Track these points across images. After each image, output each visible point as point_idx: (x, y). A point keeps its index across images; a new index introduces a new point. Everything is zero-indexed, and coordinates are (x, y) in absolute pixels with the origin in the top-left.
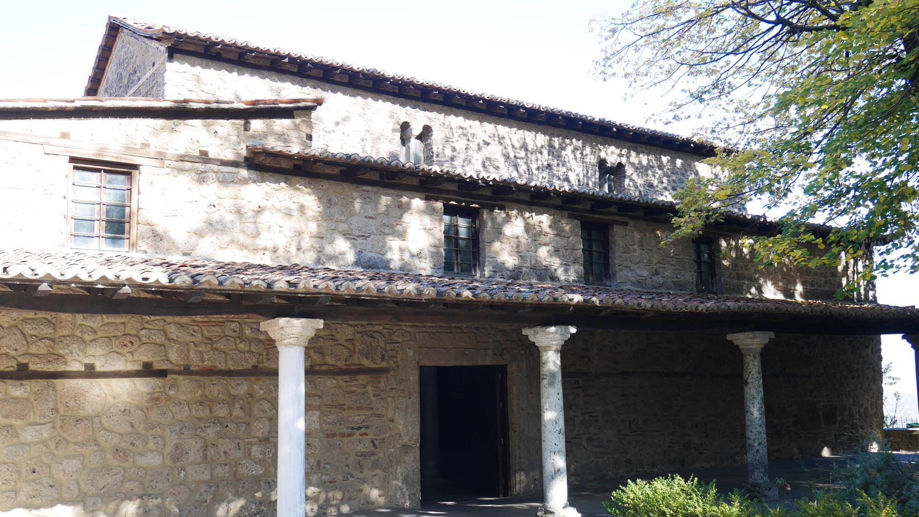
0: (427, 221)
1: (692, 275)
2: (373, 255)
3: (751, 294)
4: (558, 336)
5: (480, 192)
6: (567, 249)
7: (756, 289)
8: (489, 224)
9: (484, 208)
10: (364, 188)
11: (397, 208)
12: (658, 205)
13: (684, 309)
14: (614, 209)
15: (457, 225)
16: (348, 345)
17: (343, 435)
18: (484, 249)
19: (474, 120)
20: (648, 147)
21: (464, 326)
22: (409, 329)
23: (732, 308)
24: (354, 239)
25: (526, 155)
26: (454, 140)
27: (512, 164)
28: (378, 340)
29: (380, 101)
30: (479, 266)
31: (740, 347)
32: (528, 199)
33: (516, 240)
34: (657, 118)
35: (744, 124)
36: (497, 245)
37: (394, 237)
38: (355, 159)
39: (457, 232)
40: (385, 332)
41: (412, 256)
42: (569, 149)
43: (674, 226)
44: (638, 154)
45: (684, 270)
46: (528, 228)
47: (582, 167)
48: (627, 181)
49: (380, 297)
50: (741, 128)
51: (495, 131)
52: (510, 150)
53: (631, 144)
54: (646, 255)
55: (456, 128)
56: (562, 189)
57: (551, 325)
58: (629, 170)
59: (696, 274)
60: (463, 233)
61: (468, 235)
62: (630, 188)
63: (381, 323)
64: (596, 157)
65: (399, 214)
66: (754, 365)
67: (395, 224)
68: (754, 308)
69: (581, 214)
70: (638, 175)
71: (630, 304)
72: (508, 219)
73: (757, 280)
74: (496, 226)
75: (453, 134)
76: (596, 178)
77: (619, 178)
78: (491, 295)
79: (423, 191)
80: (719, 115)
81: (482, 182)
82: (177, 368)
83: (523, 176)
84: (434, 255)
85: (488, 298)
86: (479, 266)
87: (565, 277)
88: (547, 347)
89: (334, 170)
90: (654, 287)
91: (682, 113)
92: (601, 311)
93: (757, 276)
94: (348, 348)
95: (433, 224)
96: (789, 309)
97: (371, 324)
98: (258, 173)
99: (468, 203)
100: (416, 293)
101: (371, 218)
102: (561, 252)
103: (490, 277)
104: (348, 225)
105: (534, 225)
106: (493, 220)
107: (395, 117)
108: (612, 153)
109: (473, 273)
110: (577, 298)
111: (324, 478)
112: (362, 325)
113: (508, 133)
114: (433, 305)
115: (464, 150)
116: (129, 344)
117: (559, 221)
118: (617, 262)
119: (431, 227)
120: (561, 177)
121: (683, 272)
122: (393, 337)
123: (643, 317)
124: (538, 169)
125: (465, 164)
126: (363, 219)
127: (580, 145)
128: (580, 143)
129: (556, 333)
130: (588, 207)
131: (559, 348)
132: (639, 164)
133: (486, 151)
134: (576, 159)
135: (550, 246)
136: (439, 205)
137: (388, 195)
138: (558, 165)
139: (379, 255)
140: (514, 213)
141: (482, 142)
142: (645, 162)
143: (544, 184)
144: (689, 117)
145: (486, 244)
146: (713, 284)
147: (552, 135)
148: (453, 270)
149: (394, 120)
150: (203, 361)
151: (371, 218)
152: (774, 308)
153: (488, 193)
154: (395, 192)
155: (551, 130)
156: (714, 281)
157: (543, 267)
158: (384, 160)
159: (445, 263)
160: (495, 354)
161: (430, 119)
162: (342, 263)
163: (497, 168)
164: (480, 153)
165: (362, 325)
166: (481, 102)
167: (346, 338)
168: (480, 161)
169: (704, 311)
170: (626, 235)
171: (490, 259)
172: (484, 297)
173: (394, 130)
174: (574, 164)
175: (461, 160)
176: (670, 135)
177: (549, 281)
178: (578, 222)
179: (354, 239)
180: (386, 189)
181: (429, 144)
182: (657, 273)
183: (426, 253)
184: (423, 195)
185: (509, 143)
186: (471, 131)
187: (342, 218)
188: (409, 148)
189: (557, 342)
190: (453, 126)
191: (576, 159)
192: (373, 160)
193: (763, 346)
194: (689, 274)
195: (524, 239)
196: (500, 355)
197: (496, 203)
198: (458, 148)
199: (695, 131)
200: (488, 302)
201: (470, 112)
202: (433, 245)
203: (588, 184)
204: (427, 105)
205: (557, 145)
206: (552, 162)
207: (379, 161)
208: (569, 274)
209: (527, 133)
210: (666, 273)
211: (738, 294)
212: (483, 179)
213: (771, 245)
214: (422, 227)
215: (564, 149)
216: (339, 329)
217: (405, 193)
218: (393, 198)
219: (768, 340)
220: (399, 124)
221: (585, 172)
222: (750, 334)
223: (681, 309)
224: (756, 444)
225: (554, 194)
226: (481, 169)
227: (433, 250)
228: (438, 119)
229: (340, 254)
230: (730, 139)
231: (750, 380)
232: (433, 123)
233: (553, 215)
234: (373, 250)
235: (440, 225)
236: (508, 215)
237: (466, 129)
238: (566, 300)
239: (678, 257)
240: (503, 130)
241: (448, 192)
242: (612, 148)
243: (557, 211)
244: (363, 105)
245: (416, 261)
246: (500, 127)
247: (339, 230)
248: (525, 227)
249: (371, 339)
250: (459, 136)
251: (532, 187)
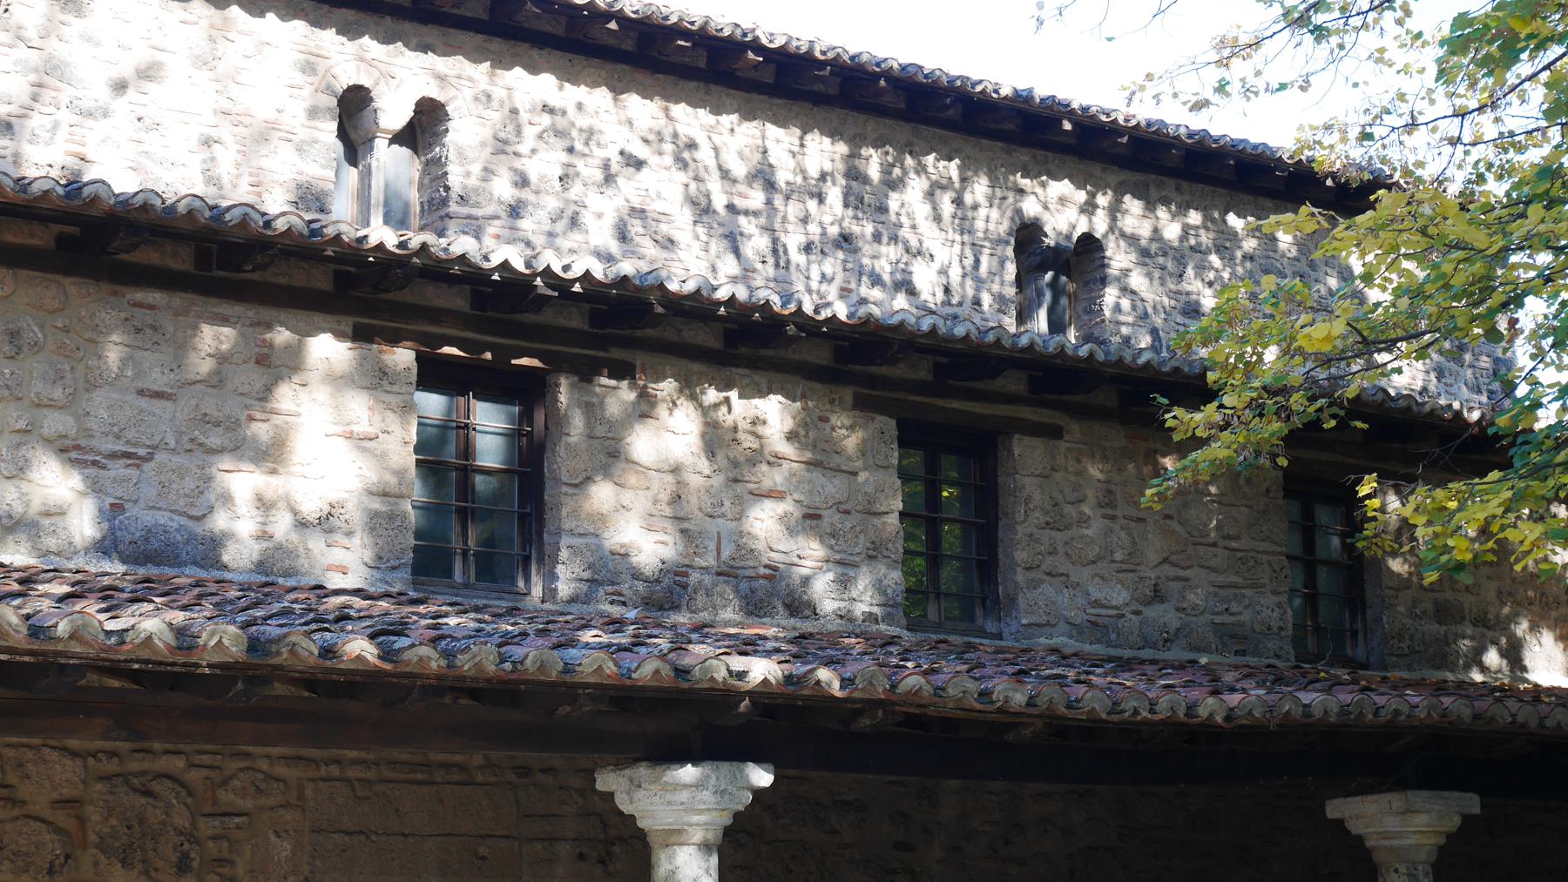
0: (360, 409)
1: (1279, 605)
2: (162, 518)
3: (1484, 669)
4: (706, 796)
5: (547, 317)
6: (847, 512)
7: (1503, 654)
8: (577, 424)
9: (559, 370)
10: (139, 295)
11: (251, 365)
12: (1158, 372)
13: (1145, 714)
14: (1013, 382)
15: (467, 426)
16: (63, 819)
18: (559, 506)
19: (594, 84)
20: (1185, 185)
21: (477, 758)
22: (281, 770)
23: (1317, 713)
24: (95, 463)
25: (769, 202)
26: (524, 148)
27: (721, 231)
28: (169, 805)
29: (271, 16)
30: (541, 561)
31: (1369, 843)
32: (716, 343)
33: (670, 478)
34: (1165, 88)
35: (1461, 114)
36: (602, 494)
37: (241, 459)
38: (95, 199)
39: (467, 450)
40: (194, 776)
41: (302, 524)
42: (916, 186)
43: (1176, 437)
44: (1150, 206)
45: (1252, 586)
46: (715, 439)
47: (957, 247)
48: (1110, 295)
49: (44, 653)
50: (1451, 127)
51: (663, 121)
52: (715, 186)
53: (1125, 175)
54: (1123, 534)
55: (532, 111)
56: (825, 314)
57: (681, 758)
58: (1119, 258)
59: (1297, 602)
60: (490, 450)
61: (509, 459)
62: (1122, 318)
63: (182, 747)
64: (1009, 213)
65: (258, 385)
67: (243, 418)
68: (1397, 712)
69: (900, 395)
70: (1149, 275)
71: (951, 691)
72: (645, 408)
73: (1504, 625)
74: (600, 431)
75: (519, 132)
76: (1002, 283)
77: (1087, 283)
78: (448, 655)
79: (346, 312)
80: (1381, 86)
81: (548, 285)
83: (754, 271)
84: (378, 523)
85: (436, 663)
86: (541, 561)
87: (835, 605)
88: (672, 832)
89: (32, 235)
90: (1148, 643)
91: (1258, 73)
92: (858, 713)
93: (1506, 610)
94: (59, 830)
95: (377, 418)
96: (1520, 719)
97: (147, 751)
99: (504, 354)
100: (173, 643)
101: (158, 395)
102: (826, 520)
103: (573, 600)
104: (78, 418)
105: (735, 429)
106: (592, 410)
107: (321, 71)
108: (1062, 200)
109: (521, 584)
110: (761, 670)
112: (112, 754)
113: (710, 130)
114: (240, 685)
115: (557, 184)
117: (825, 420)
118: (1021, 556)
119: (372, 430)
120: (886, 278)
121: (1249, 592)
122: (222, 794)
123: (1010, 737)
124: (808, 248)
125: (560, 227)
126: (131, 398)
127: (955, 174)
128: (953, 168)
129: (699, 785)
130: (923, 373)
131: (713, 836)
132: (1152, 240)
133: (631, 188)
134: (937, 218)
135: (789, 499)
136: (403, 357)
137: (224, 321)
138: (877, 237)
139: (184, 521)
140: (666, 387)
141: (615, 159)
142: (1172, 231)
143: (762, 295)
144: (1283, 87)
145: (564, 489)
146: (1354, 634)
147: (856, 141)
148: (448, 573)
149: (316, 80)
151: (158, 395)
152: (1466, 713)
153: (576, 321)
154: (251, 313)
155: (856, 121)
156: (1359, 626)
157: (762, 571)
158: (198, 203)
159: (416, 549)
160: (581, 857)
161: (441, 78)
162: (51, 543)
163: (669, 243)
164: (609, 192)
165: (112, 754)
166: (613, 25)
167: (55, 796)
168: (610, 220)
169: (1219, 719)
170: (1053, 469)
171: (577, 541)
172: (421, 659)
173: (313, 113)
174: (931, 237)
175: (542, 215)
176: (1255, 147)
177: (782, 617)
178: (890, 424)
179: (95, 463)
180: (216, 301)
181: (438, 162)
182: (1158, 596)
183: (354, 513)
184: (347, 323)
185: (712, 163)
186: (583, 122)
187: (58, 393)
188: (370, 173)
189: (702, 818)
190: (522, 103)
191: (937, 218)
192: (158, 202)
193: (1442, 840)
194: (1270, 600)
195: (700, 471)
196: (602, 862)
197: (602, 354)
198: (533, 178)
199: (1308, 136)
200: (439, 677)
201: (579, 60)
202: (375, 489)
203: (977, 302)
204: (431, 33)
205: (874, 171)
206: (856, 229)
207: (182, 208)
208: (854, 594)
209: (772, 130)
210: (1191, 597)
211: (1438, 668)
212: (547, 272)
213: (1453, 505)
214: (339, 429)
215: (894, 184)
216: (30, 766)
217: (283, 315)
218: (243, 335)
219: (1457, 820)
220: (334, 93)
221: (969, 262)
222: (1396, 800)
223: (1136, 712)
225: (800, 327)
226: (614, 247)
227: (377, 505)
228: (470, 79)
229: (48, 514)
230: (1420, 164)
232: (453, 92)
233: (803, 397)
234: (161, 504)
235: (404, 425)
236: (644, 395)
237: (564, 113)
238: (721, 674)
239: (1233, 544)
240: (691, 119)
241: (435, 315)
242: (1062, 187)
243: (818, 386)
244: (212, 26)
245: (316, 543)
246: (680, 110)
247: (46, 432)
248: (703, 435)
249: (143, 800)
250: (540, 137)
251: (719, 303)
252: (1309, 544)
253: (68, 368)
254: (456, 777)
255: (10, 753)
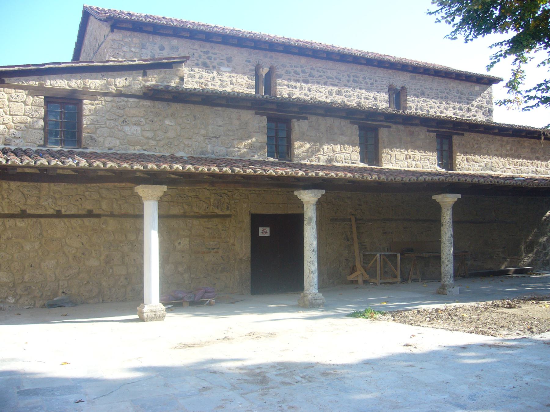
10: (216, 108)
17: (204, 253)
22: (244, 192)
40: (229, 193)
66: (447, 214)
79: (253, 109)
82: (106, 213)
98: (152, 101)
101: (220, 126)
111: (192, 276)
116: (80, 200)
130: (363, 117)
149: (250, 64)
150: (121, 209)
151: (220, 126)
158: (225, 92)
167: (205, 197)
179: (210, 139)
187: (203, 126)
193: (454, 203)
219: (456, 199)
224: (446, 261)
231: (444, 224)
247: (201, 133)
249: (221, 198)
252: (442, 147)
253: (204, 122)
254: (276, 193)
255: (197, 190)
